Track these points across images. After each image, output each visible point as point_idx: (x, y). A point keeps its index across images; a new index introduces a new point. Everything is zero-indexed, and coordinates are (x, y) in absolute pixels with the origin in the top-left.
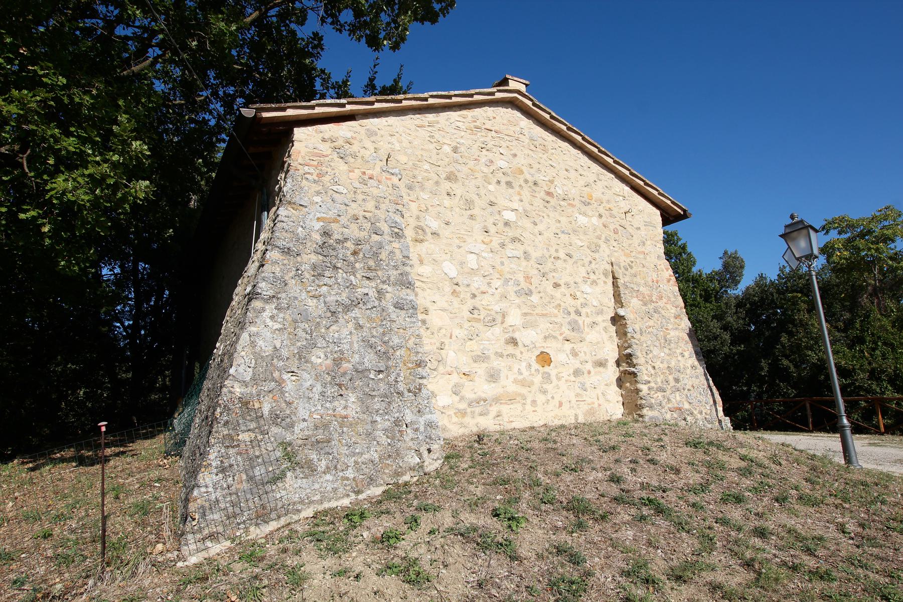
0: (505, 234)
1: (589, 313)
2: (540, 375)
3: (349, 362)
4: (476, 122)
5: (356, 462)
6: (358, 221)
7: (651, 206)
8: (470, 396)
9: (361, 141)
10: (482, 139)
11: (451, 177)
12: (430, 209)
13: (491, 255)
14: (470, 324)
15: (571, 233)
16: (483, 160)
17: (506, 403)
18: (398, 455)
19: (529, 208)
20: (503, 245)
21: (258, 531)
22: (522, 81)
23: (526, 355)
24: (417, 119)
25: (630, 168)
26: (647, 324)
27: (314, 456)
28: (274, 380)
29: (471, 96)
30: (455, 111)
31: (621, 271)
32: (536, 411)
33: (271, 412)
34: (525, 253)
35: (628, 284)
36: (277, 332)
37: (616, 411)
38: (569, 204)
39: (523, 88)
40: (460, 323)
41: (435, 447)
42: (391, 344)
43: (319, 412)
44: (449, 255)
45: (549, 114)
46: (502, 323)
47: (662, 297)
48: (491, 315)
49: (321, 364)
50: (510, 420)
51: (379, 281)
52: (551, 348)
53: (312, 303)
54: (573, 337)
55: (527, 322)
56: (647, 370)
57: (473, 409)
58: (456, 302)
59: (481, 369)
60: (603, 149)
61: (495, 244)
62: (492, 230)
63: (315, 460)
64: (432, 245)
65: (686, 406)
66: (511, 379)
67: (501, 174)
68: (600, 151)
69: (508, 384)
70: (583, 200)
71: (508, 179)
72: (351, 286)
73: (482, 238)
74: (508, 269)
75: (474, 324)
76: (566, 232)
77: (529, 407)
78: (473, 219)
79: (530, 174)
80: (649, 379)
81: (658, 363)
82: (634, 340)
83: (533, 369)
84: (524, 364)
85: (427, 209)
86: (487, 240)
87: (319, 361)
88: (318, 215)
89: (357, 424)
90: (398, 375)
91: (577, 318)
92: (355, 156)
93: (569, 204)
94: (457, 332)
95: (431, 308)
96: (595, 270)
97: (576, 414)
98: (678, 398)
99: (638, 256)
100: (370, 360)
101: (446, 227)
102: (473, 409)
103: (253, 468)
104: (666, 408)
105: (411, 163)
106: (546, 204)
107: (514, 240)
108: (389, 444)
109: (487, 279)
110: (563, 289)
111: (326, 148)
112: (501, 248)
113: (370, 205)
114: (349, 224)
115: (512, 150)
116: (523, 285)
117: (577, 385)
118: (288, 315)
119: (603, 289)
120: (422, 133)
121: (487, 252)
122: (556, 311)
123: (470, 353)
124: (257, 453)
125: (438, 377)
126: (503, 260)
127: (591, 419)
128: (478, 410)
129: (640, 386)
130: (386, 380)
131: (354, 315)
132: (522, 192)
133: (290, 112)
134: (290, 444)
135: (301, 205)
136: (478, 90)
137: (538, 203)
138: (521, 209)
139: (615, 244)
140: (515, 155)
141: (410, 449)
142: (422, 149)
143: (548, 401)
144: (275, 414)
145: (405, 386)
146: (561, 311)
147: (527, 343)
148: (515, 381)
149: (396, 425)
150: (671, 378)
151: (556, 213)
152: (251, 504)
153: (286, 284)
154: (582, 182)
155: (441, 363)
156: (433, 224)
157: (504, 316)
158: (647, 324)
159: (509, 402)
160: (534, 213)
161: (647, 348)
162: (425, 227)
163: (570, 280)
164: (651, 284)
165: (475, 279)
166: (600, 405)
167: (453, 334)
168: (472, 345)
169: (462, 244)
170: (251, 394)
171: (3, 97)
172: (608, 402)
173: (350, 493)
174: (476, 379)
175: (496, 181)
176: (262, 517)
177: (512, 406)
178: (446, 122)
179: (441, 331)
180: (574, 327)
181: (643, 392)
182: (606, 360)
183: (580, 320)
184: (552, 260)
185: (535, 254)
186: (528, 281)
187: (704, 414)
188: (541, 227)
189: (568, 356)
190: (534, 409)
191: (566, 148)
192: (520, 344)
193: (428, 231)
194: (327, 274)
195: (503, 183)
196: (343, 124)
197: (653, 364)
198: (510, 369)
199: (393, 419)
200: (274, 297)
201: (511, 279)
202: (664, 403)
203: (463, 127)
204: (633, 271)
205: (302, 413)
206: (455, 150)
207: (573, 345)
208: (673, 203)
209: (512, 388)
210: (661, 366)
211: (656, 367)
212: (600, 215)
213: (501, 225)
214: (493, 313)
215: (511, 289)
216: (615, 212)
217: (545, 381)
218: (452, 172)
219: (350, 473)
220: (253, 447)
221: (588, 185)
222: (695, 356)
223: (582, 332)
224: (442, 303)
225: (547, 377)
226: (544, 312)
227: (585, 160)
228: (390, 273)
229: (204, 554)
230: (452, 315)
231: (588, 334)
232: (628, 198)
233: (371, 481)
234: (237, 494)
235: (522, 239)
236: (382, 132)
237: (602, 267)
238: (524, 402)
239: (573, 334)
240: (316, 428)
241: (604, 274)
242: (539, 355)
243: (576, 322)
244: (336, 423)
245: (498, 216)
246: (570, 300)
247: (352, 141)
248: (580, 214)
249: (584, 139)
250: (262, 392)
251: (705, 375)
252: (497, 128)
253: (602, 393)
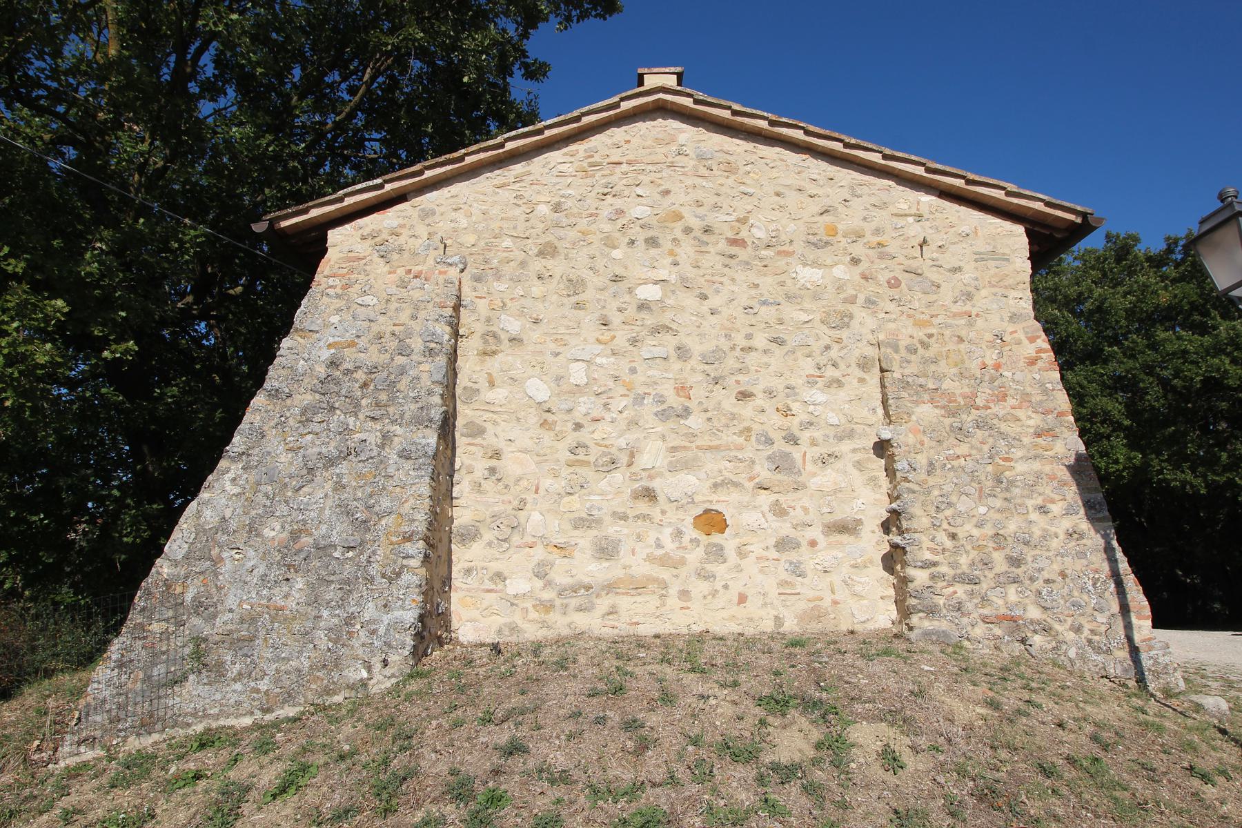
0: (639, 323)
3: (311, 535)
4: (592, 156)
5: (278, 671)
6: (383, 340)
7: (998, 221)
8: (561, 579)
9: (412, 227)
10: (603, 181)
11: (548, 251)
12: (509, 303)
13: (612, 359)
14: (571, 470)
15: (782, 302)
16: (605, 212)
17: (627, 594)
18: (336, 665)
19: (690, 272)
20: (634, 342)
21: (137, 742)
22: (667, 70)
23: (672, 516)
24: (497, 176)
25: (923, 160)
26: (951, 452)
27: (228, 658)
28: (210, 559)
29: (578, 119)
30: (559, 149)
31: (897, 357)
32: (688, 608)
33: (194, 599)
34: (679, 348)
35: (910, 380)
36: (234, 498)
37: (884, 616)
38: (779, 253)
39: (671, 81)
40: (553, 469)
41: (394, 658)
42: (377, 508)
43: (251, 600)
44: (538, 368)
45: (729, 108)
46: (629, 465)
47: (1005, 396)
48: (609, 453)
49: (273, 539)
50: (634, 621)
51: (387, 421)
52: (726, 503)
53: (284, 458)
54: (776, 483)
55: (677, 461)
56: (932, 540)
57: (565, 601)
58: (547, 437)
59: (585, 540)
60: (853, 141)
61: (621, 341)
62: (616, 319)
63: (228, 663)
64: (510, 358)
65: (1034, 613)
66: (642, 553)
67: (638, 228)
68: (847, 145)
69: (635, 562)
70: (812, 239)
71: (650, 233)
72: (346, 431)
73: (597, 335)
74: (643, 379)
75: (578, 469)
76: (771, 301)
77: (673, 601)
78: (580, 309)
79: (696, 217)
80: (936, 559)
82: (907, 485)
83: (686, 539)
84: (668, 531)
85: (505, 305)
86: (607, 336)
87: (273, 534)
88: (331, 340)
89: (294, 618)
90: (374, 553)
91: (788, 448)
92: (401, 250)
93: (779, 253)
94: (547, 483)
95: (507, 450)
96: (839, 360)
97: (776, 617)
99: (950, 321)
100: (339, 532)
101: (534, 327)
102: (565, 601)
103: (154, 665)
104: (975, 615)
105: (482, 243)
106: (728, 261)
107: (656, 330)
108: (329, 650)
109: (603, 399)
110: (760, 401)
111: (364, 248)
112: (631, 348)
113: (404, 317)
114: (368, 345)
115: (660, 185)
116: (674, 401)
117: (783, 565)
118: (252, 476)
119: (857, 393)
120: (506, 195)
121: (607, 356)
122: (741, 440)
123: (568, 515)
124: (164, 649)
125: (511, 551)
126: (633, 365)
127: (814, 627)
128: (574, 602)
129: (911, 572)
130: (357, 559)
131: (338, 471)
132: (678, 250)
133: (314, 213)
134: (205, 640)
135: (310, 331)
136: (585, 109)
137: (712, 260)
138: (673, 278)
139: (891, 307)
140: (667, 192)
141: (356, 658)
142: (502, 219)
143: (714, 593)
144: (199, 602)
145: (381, 568)
146: (753, 439)
147: (675, 495)
148: (650, 559)
149: (346, 624)
150: (998, 557)
151: (748, 273)
152: (139, 709)
153: (263, 436)
154: (815, 207)
155: (516, 530)
156: (513, 325)
157: (632, 455)
158: (951, 452)
159: (633, 592)
160: (702, 280)
161: (940, 499)
162: (499, 332)
163: (778, 384)
164: (978, 373)
165: (581, 399)
166: (835, 603)
167: (541, 486)
168: (575, 504)
169: (561, 349)
170: (178, 575)
172: (856, 598)
173: (256, 711)
174: (576, 554)
175: (627, 240)
176: (146, 726)
177: (639, 599)
178: (542, 170)
179: (521, 483)
180: (781, 464)
181: (916, 583)
182: (859, 522)
183: (796, 454)
184: (738, 352)
185: (697, 348)
186: (681, 394)
188: (715, 301)
189: (764, 516)
190: (685, 604)
191: (775, 157)
192: (661, 498)
193: (503, 336)
194: (318, 418)
195: (640, 243)
196: (390, 210)
197: (952, 530)
198: (639, 537)
199: (345, 615)
200: (243, 453)
201: (649, 394)
202: (969, 606)
203: (571, 170)
204: (930, 353)
205: (231, 602)
206: (557, 208)
208: (1048, 204)
209: (641, 568)
210: (976, 532)
211: (960, 535)
212: (853, 259)
213: (631, 311)
214: (613, 450)
215: (649, 409)
216: (893, 248)
217: (712, 558)
218: (548, 243)
219: (263, 685)
220: (161, 641)
221: (826, 211)
222: (1082, 511)
223: (799, 473)
224: (525, 440)
226: (715, 443)
228: (406, 408)
229: (77, 759)
230: (539, 458)
232: (932, 216)
233: (289, 697)
234: (127, 695)
235: (674, 326)
236: (442, 209)
237: (857, 353)
238: (664, 592)
239: (779, 477)
240: (242, 621)
241: (859, 365)
242: (700, 515)
243: (786, 456)
244: (267, 616)
245: (628, 296)
246: (777, 419)
247: (399, 230)
248: (805, 265)
249: (807, 132)
250: (192, 574)
251: (1109, 550)
252: (631, 157)
253: (844, 581)
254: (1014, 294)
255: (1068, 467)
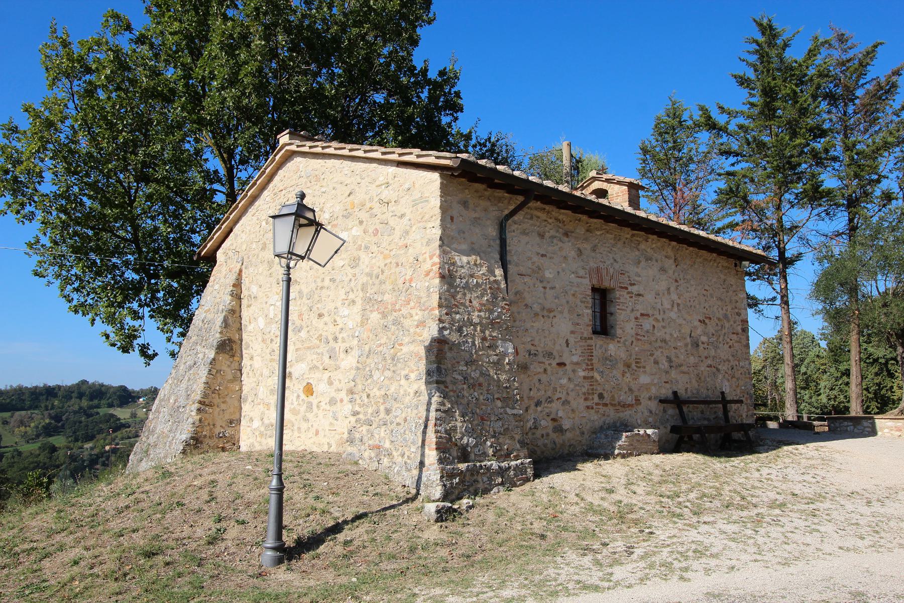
1: (346, 338)
2: (305, 405)
65: (387, 445)
81: (375, 390)
98: (382, 435)
104: (367, 445)
171: (602, 201)
187: (406, 457)
202: (365, 439)
207: (330, 374)
225: (310, 407)
227: (251, 211)
231: (343, 360)
254: (430, 225)
255: (425, 347)
